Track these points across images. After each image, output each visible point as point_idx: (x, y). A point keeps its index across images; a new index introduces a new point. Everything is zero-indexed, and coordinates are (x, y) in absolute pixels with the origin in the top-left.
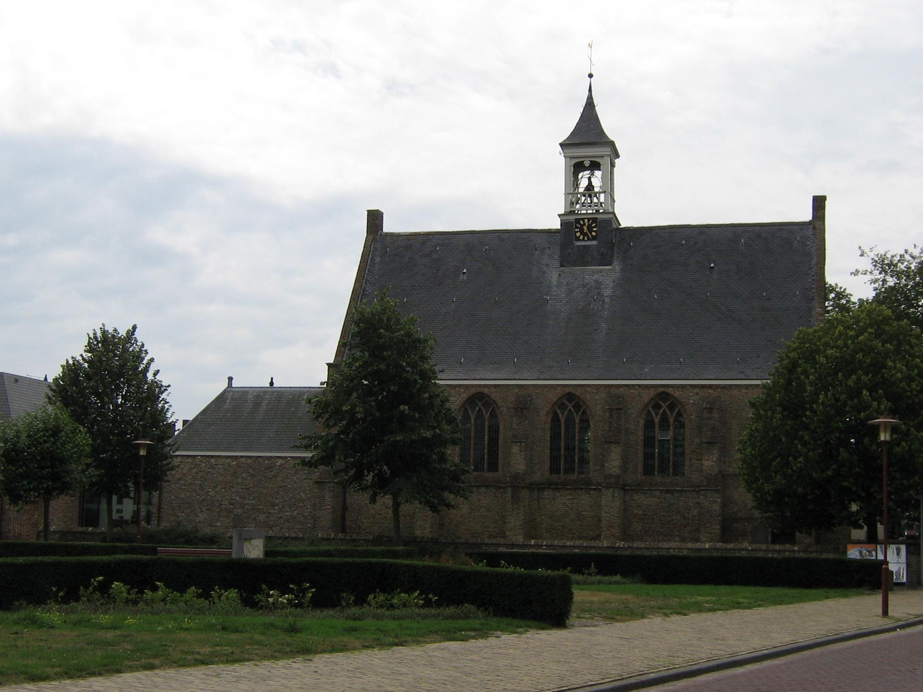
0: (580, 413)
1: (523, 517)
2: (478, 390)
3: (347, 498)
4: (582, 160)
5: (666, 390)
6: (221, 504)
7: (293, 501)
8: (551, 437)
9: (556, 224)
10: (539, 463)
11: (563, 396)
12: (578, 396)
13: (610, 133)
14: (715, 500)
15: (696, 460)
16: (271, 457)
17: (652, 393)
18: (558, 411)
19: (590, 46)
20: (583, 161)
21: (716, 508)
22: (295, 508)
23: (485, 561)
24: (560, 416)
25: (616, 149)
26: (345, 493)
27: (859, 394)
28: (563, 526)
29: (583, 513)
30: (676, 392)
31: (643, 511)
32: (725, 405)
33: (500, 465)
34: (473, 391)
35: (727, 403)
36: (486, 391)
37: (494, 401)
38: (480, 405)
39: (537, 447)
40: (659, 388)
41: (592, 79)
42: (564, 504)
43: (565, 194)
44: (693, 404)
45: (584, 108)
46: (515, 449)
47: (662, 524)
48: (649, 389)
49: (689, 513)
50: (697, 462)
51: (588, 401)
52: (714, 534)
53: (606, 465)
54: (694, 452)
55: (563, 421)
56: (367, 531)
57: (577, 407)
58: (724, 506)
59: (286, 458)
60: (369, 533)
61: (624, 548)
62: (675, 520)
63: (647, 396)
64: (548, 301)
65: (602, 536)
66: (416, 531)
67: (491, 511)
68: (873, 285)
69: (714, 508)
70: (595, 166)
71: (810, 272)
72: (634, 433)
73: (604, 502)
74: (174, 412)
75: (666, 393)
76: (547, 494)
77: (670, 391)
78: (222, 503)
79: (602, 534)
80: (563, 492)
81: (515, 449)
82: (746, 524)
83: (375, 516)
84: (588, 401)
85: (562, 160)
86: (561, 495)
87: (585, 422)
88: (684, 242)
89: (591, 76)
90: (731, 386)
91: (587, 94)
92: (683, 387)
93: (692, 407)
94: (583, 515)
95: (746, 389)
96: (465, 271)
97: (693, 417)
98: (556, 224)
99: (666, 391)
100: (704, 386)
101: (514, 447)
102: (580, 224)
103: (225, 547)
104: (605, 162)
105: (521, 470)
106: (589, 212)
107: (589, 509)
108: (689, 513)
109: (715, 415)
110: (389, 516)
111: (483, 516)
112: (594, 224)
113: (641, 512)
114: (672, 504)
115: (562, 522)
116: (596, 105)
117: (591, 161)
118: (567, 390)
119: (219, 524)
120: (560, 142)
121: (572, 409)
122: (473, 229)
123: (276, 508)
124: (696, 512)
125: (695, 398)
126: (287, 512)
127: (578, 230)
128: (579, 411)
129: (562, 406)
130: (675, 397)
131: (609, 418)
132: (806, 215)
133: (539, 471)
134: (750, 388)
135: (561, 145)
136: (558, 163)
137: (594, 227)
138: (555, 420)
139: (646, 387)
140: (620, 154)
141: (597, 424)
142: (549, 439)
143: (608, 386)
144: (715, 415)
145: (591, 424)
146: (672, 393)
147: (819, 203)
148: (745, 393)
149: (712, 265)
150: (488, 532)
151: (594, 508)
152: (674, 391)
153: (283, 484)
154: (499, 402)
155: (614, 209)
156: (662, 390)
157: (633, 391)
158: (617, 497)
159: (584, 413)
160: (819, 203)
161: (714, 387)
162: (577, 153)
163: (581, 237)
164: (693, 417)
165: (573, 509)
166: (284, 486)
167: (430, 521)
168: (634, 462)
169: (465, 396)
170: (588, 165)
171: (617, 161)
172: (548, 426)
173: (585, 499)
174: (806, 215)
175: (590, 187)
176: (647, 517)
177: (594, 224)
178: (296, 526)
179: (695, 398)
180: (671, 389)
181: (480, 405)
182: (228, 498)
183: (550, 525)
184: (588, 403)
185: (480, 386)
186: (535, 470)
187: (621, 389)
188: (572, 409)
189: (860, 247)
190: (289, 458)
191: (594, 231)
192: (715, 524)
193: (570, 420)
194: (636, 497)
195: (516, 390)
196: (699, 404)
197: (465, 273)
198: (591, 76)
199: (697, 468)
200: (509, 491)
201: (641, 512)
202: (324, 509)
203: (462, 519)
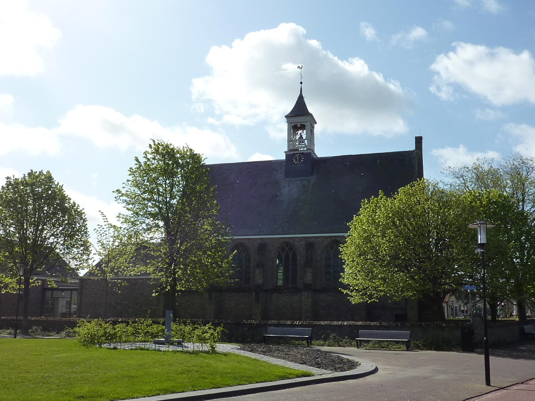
4: (296, 124)
5: (336, 239)
6: (111, 304)
9: (283, 157)
16: (136, 279)
18: (281, 252)
24: (282, 254)
25: (314, 118)
27: (180, 338)
29: (293, 305)
36: (244, 242)
40: (332, 238)
41: (302, 85)
43: (288, 141)
45: (298, 99)
46: (257, 272)
57: (291, 249)
59: (144, 279)
68: (85, 214)
70: (303, 127)
71: (414, 176)
74: (93, 258)
75: (336, 240)
78: (111, 303)
81: (257, 272)
87: (294, 255)
88: (348, 163)
96: (238, 182)
98: (283, 157)
99: (336, 239)
102: (295, 156)
103: (71, 340)
104: (308, 125)
106: (305, 149)
112: (303, 156)
116: (304, 97)
117: (301, 124)
119: (110, 314)
120: (285, 115)
123: (138, 305)
126: (143, 307)
127: (294, 159)
129: (283, 249)
132: (411, 147)
135: (286, 117)
136: (284, 126)
137: (302, 157)
140: (421, 136)
143: (306, 237)
147: (419, 141)
149: (362, 174)
153: (142, 293)
156: (334, 238)
157: (319, 240)
160: (419, 141)
162: (301, 120)
166: (142, 294)
170: (300, 126)
174: (411, 147)
175: (301, 137)
177: (303, 156)
182: (115, 300)
187: (313, 239)
189: (207, 158)
190: (145, 279)
191: (303, 159)
195: (259, 241)
197: (238, 183)
198: (301, 83)
200: (254, 294)
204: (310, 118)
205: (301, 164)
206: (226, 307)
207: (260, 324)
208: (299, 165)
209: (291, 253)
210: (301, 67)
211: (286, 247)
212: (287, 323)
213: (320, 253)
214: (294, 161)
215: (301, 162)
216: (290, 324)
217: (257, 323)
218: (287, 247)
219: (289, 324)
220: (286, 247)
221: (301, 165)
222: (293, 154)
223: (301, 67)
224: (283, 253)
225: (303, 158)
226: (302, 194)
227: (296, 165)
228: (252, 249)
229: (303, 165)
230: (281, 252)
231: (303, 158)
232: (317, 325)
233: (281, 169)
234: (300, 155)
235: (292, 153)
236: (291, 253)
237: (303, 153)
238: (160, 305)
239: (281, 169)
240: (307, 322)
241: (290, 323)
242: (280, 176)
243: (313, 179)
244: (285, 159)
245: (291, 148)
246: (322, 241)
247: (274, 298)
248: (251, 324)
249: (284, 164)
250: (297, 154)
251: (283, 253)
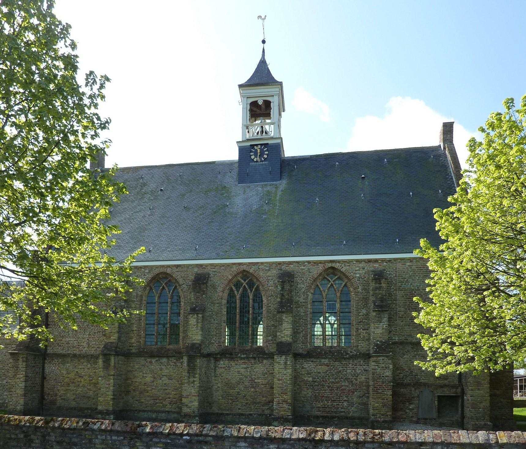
0: (254, 290)
1: (198, 384)
2: (162, 270)
3: (46, 368)
5: (333, 265)
7: (3, 371)
8: (227, 312)
9: (233, 155)
10: (215, 335)
11: (238, 274)
12: (251, 274)
13: (277, 78)
14: (387, 365)
15: (363, 330)
17: (321, 267)
18: (234, 288)
19: (264, 42)
20: (257, 101)
21: (388, 373)
22: (4, 378)
23: (419, 336)
24: (236, 292)
26: (44, 364)
28: (238, 392)
29: (256, 381)
30: (343, 267)
31: (313, 378)
32: (390, 278)
33: (181, 338)
34: (156, 271)
35: (392, 277)
36: (169, 271)
37: (176, 280)
38: (164, 284)
39: (214, 320)
40: (327, 264)
42: (239, 372)
44: (359, 278)
46: (192, 320)
47: (331, 390)
48: (317, 265)
49: (356, 380)
50: (364, 331)
51: (261, 277)
52: (387, 399)
53: (278, 334)
54: (360, 322)
55: (238, 297)
56: (62, 397)
57: (251, 284)
58: (394, 371)
60: (64, 399)
61: (332, 441)
62: (343, 386)
63: (316, 271)
64: (227, 206)
65: (275, 402)
66: (99, 398)
67: (172, 379)
69: (387, 374)
72: (303, 306)
73: (276, 370)
76: (222, 363)
77: (337, 266)
79: (275, 400)
80: (237, 361)
81: (192, 320)
82: (413, 389)
83: (69, 384)
84: (261, 277)
85: (239, 98)
86: (236, 364)
87: (258, 298)
89: (264, 42)
90: (395, 260)
91: (261, 56)
92: (349, 261)
93: (358, 280)
94: (256, 382)
95: (411, 261)
97: (360, 290)
100: (369, 261)
101: (192, 319)
105: (198, 340)
107: (262, 377)
108: (356, 380)
109: (383, 285)
110: (82, 384)
111: (165, 384)
112: (266, 149)
113: (311, 379)
114: (340, 371)
115: (237, 389)
118: (242, 268)
121: (246, 286)
122: (171, 163)
124: (363, 378)
125: (361, 272)
128: (253, 287)
129: (238, 285)
130: (342, 272)
131: (280, 291)
133: (216, 342)
134: (415, 260)
137: (266, 151)
138: (231, 295)
139: (315, 263)
141: (269, 298)
142: (226, 313)
143: (280, 263)
144: (383, 285)
145: (264, 299)
146: (339, 268)
148: (409, 266)
150: (169, 398)
151: (266, 375)
152: (341, 266)
154: (181, 281)
155: (280, 134)
156: (330, 265)
158: (289, 365)
159: (257, 289)
161: (379, 262)
163: (255, 160)
164: (360, 290)
165: (247, 377)
167: (112, 388)
168: (304, 332)
169: (150, 276)
170: (261, 103)
171: (283, 113)
172: (224, 302)
173: (260, 368)
176: (316, 384)
177: (266, 149)
178: (5, 393)
179: (361, 272)
180: (338, 264)
181: (164, 284)
183: (225, 392)
184: (261, 280)
185: (163, 266)
186: (212, 341)
187: (292, 266)
188: (246, 286)
191: (266, 154)
192: (387, 389)
193: (244, 296)
194: (306, 365)
195: (196, 270)
196: (366, 277)
199: (364, 337)
200: (185, 359)
201: (311, 379)
202: (17, 378)
203: (146, 387)
204: (278, 89)
205: (262, 161)
206: (136, 382)
207: (201, 435)
208: (260, 163)
209: (251, 291)
210: (263, 17)
211: (242, 281)
212: (291, 434)
213: (303, 290)
214: (253, 157)
215: (264, 158)
216: (303, 439)
217: (191, 432)
218: (245, 281)
219: (299, 440)
220: (242, 281)
221: (264, 163)
222: (251, 145)
223: (263, 17)
224: (238, 291)
225: (267, 153)
226: (266, 204)
227: (256, 163)
228: (184, 284)
229: (266, 162)
230: (234, 288)
231: (267, 153)
232: (399, 442)
233: (230, 172)
234: (261, 147)
235: (249, 144)
236: (251, 291)
237: (268, 144)
238: (18, 376)
239: (230, 172)
240: (361, 431)
241: (301, 436)
242: (230, 180)
243: (283, 184)
244: (238, 159)
245: (248, 137)
246: (309, 269)
247: (221, 368)
248: (174, 434)
249: (237, 165)
250: (257, 145)
251: (238, 291)
